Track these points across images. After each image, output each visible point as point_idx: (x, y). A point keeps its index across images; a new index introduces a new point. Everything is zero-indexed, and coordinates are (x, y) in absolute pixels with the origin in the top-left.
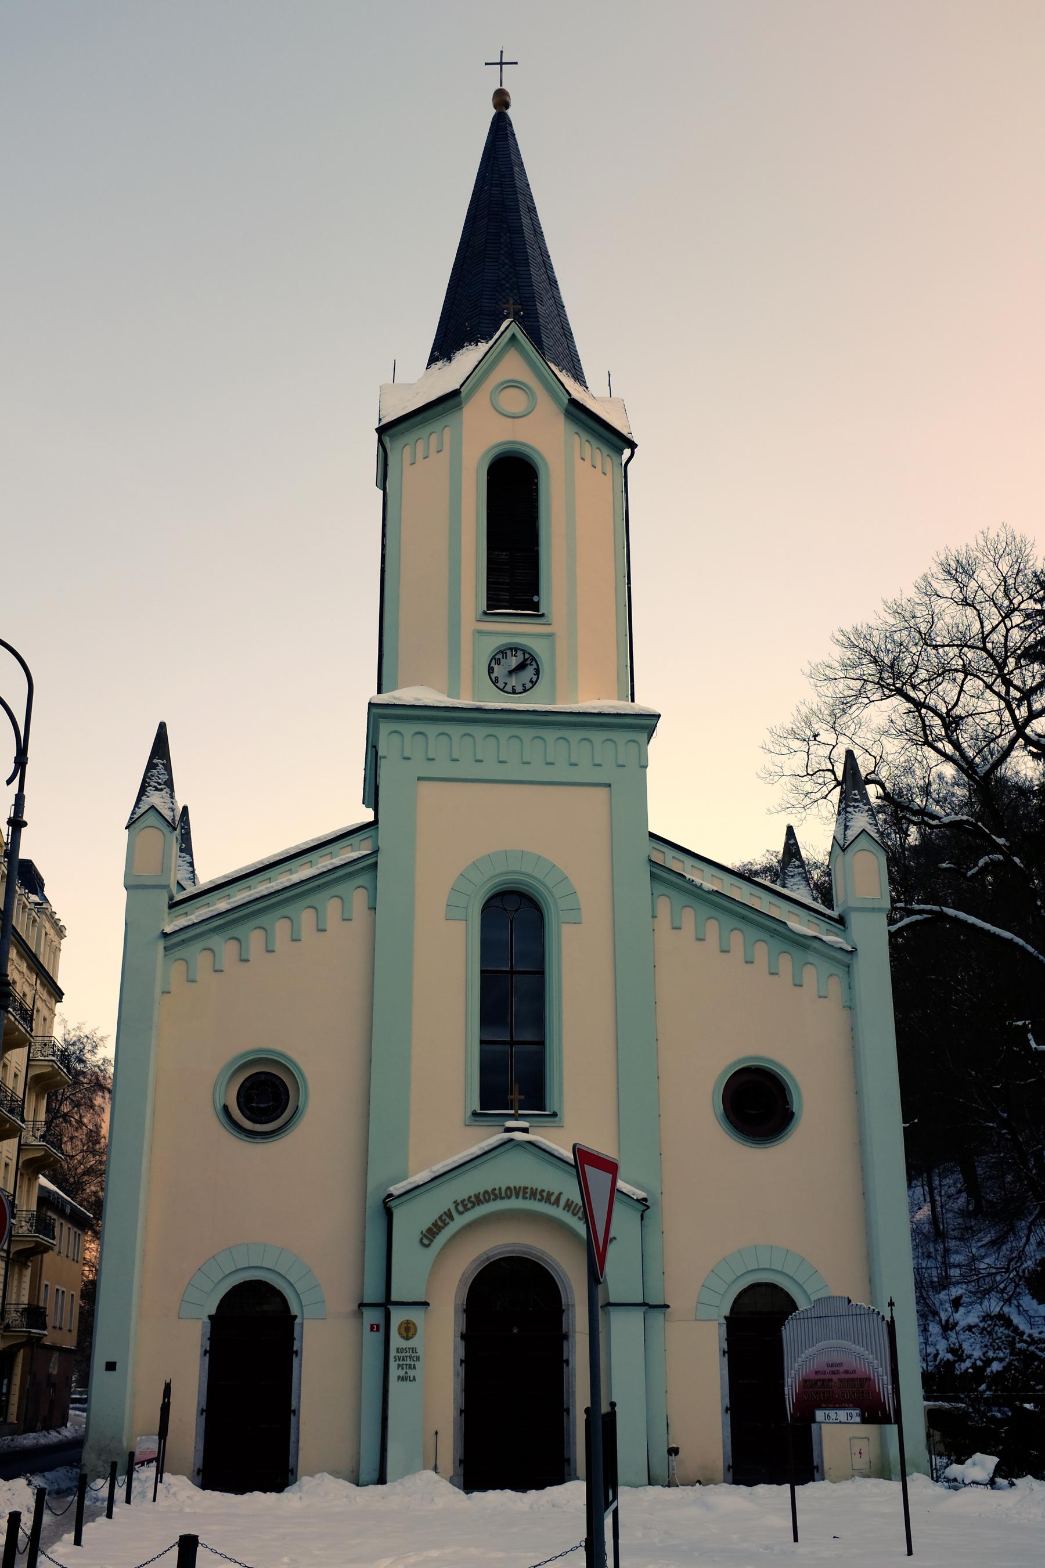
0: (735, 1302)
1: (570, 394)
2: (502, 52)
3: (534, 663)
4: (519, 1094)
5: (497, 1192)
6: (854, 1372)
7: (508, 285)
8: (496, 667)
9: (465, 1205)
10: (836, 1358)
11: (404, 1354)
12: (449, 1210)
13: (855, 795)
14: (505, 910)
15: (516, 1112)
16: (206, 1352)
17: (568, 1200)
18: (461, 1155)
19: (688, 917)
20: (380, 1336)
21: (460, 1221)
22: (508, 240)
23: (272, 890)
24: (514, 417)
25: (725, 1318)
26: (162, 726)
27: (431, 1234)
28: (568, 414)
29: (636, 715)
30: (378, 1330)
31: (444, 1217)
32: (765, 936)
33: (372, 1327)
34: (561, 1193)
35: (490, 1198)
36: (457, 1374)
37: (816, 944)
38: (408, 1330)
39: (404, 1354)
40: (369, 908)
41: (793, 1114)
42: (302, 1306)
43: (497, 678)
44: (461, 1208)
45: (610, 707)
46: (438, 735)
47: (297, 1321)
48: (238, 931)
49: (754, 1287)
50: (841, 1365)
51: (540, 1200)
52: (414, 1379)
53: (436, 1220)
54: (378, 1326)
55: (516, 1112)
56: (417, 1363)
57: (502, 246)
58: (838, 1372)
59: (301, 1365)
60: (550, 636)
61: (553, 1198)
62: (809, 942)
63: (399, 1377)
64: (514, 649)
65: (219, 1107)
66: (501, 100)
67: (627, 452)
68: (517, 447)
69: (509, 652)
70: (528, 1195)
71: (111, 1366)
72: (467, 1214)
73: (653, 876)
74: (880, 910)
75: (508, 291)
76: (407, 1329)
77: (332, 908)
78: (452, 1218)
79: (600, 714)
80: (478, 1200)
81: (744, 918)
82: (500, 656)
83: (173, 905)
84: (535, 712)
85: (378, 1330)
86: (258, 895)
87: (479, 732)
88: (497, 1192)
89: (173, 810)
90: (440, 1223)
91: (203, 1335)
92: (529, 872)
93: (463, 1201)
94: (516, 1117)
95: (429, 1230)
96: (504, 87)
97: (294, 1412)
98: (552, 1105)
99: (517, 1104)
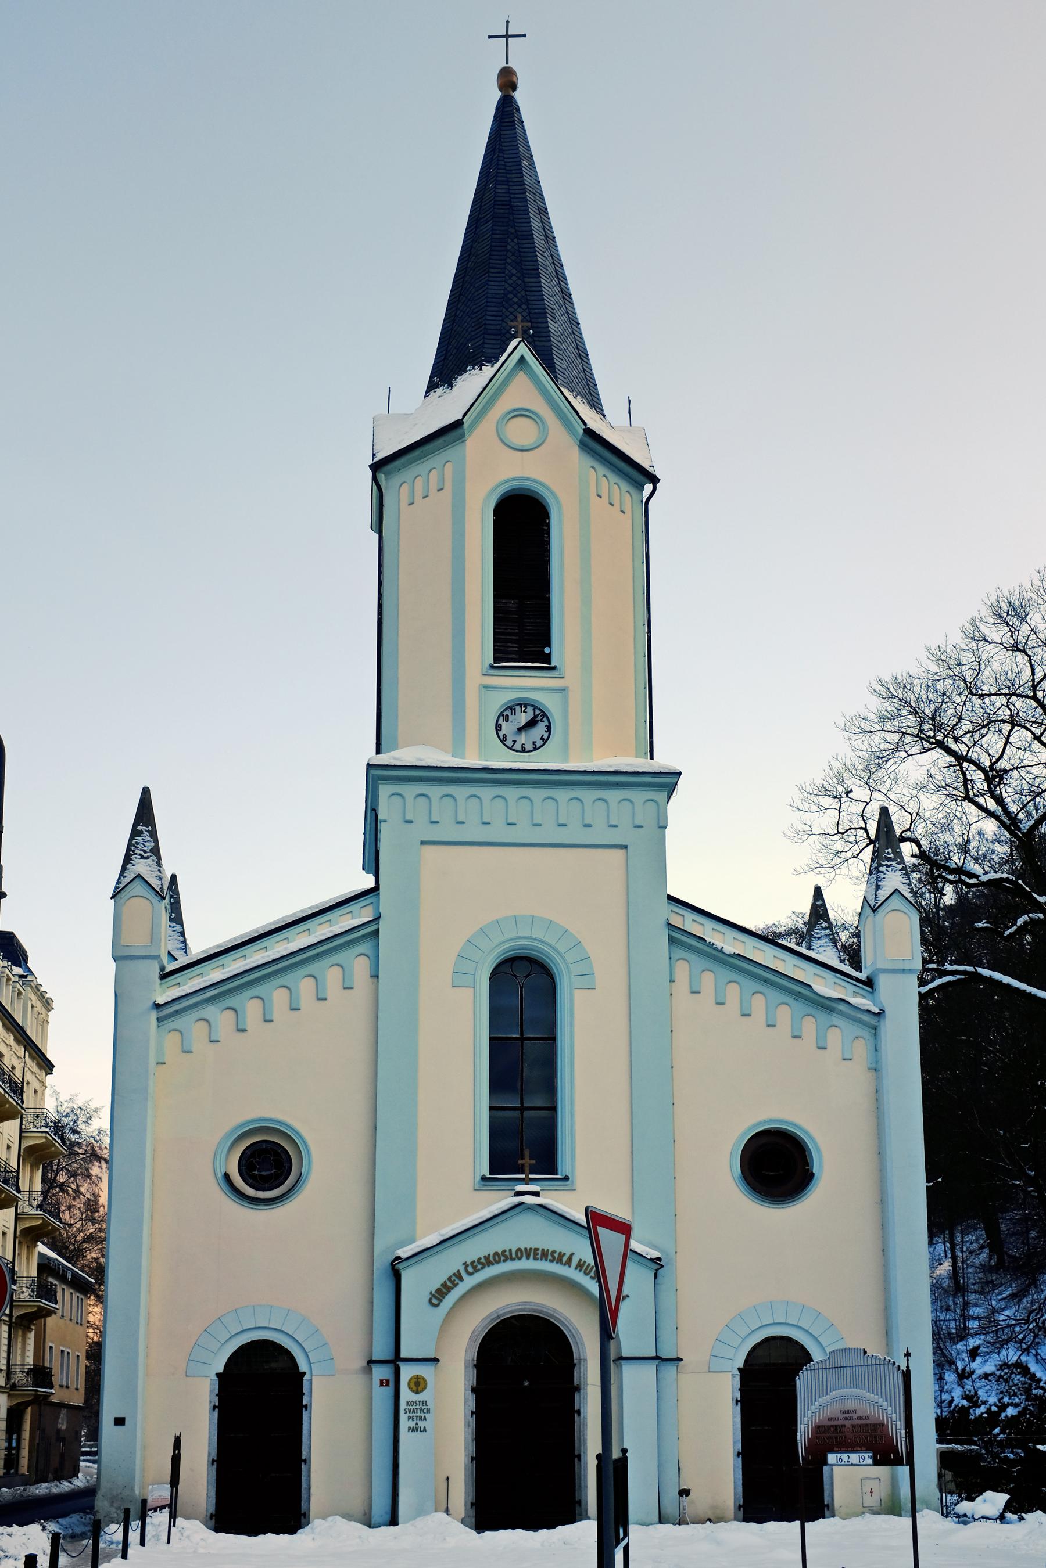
0: (749, 1355)
2: (508, 22)
3: (545, 719)
5: (507, 1253)
6: (868, 1418)
7: (516, 300)
8: (504, 724)
9: (474, 1267)
10: (849, 1405)
11: (414, 1407)
13: (888, 853)
14: (515, 976)
15: (527, 1176)
16: (215, 1407)
17: (580, 1260)
19: (708, 981)
20: (389, 1390)
21: (469, 1282)
22: (516, 247)
24: (522, 451)
25: (739, 1369)
26: (146, 792)
27: (440, 1294)
28: (583, 445)
30: (387, 1385)
31: (453, 1278)
32: (789, 999)
33: (381, 1382)
34: (572, 1254)
35: (500, 1259)
36: (467, 1425)
37: (842, 1007)
38: (418, 1384)
39: (414, 1407)
40: (371, 977)
41: (813, 1175)
42: (310, 1364)
43: (505, 736)
44: (470, 1269)
47: (306, 1378)
48: (233, 1001)
50: (854, 1411)
51: (552, 1261)
53: (445, 1282)
54: (387, 1381)
55: (527, 1176)
57: (509, 254)
58: (851, 1419)
60: (563, 690)
62: (834, 1005)
63: (409, 1428)
64: (524, 705)
65: (220, 1175)
66: (507, 80)
67: (648, 488)
69: (518, 709)
70: (539, 1256)
72: (476, 1275)
73: (671, 939)
74: (911, 971)
75: (516, 306)
76: (417, 1384)
77: (332, 976)
78: (461, 1279)
79: (616, 773)
80: (488, 1261)
82: (508, 712)
85: (387, 1385)
88: (507, 1253)
89: (160, 879)
90: (449, 1284)
91: (211, 1391)
93: (472, 1263)
95: (438, 1291)
96: (510, 65)
99: (527, 1169)
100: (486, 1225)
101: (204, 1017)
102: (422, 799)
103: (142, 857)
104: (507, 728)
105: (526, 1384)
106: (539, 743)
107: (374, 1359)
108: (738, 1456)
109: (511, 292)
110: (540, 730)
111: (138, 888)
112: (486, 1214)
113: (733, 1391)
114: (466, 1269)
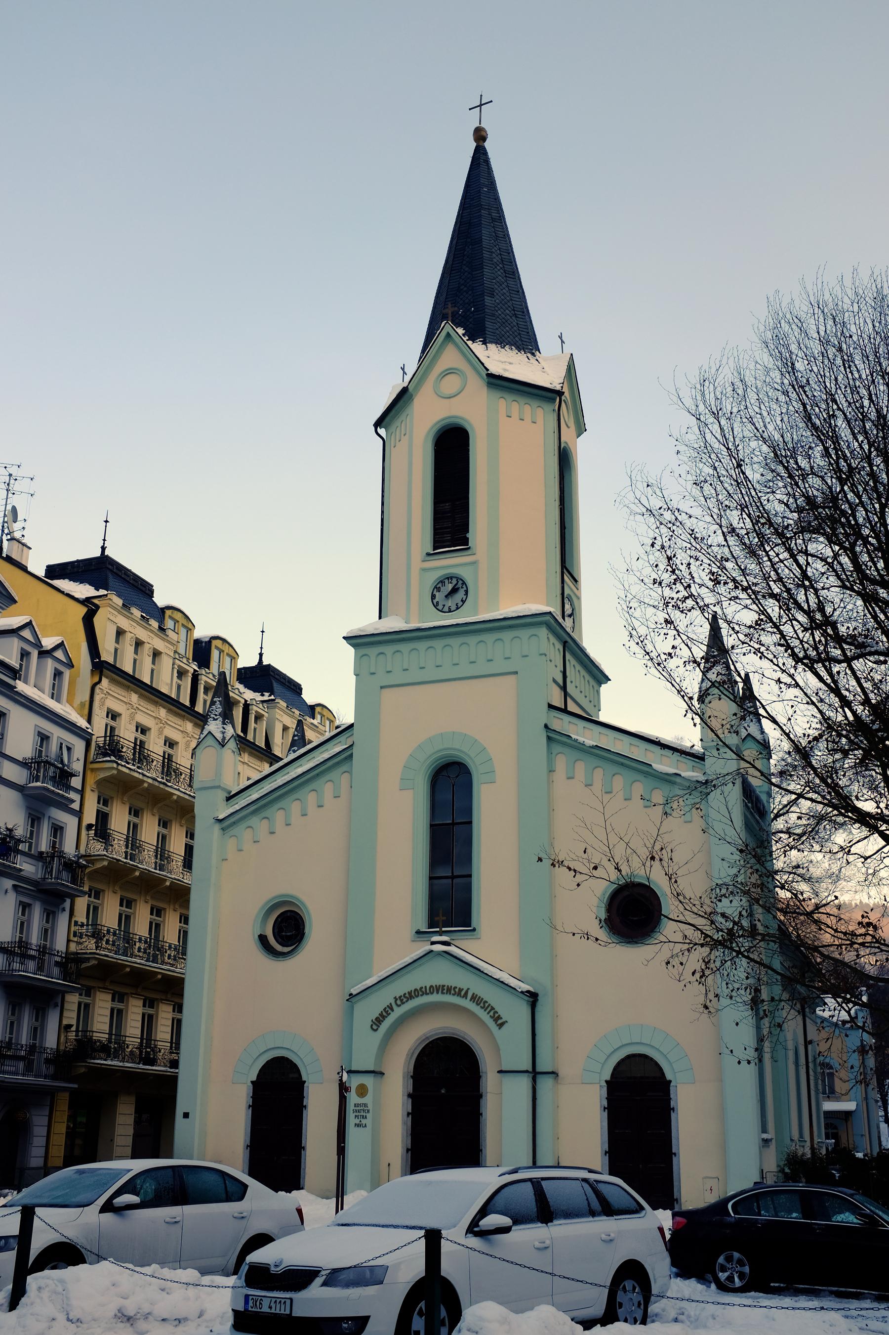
0: (615, 1069)
1: (487, 370)
2: (481, 96)
3: (464, 586)
4: (443, 916)
5: (424, 990)
9: (401, 1000)
11: (359, 1108)
12: (391, 1004)
13: (713, 652)
14: (449, 777)
15: (441, 929)
16: (250, 1106)
17: (474, 994)
18: (397, 964)
19: (581, 768)
21: (398, 1012)
23: (285, 781)
24: (450, 398)
25: (606, 1081)
27: (378, 1021)
28: (490, 385)
29: (532, 615)
31: (387, 1009)
32: (640, 777)
34: (468, 989)
36: (404, 1123)
37: (678, 780)
39: (359, 1108)
43: (438, 603)
44: (399, 1002)
45: (513, 612)
46: (512, 640)
48: (267, 813)
49: (630, 1057)
51: (454, 995)
52: (366, 1126)
55: (441, 929)
56: (368, 1115)
59: (677, 1120)
60: (474, 563)
61: (463, 993)
62: (673, 779)
63: (356, 1124)
64: (450, 578)
66: (480, 135)
68: (444, 422)
69: (446, 581)
70: (445, 991)
71: (186, 1115)
72: (403, 1006)
77: (328, 789)
78: (392, 1010)
79: (505, 619)
81: (622, 764)
83: (228, 799)
84: (457, 625)
86: (276, 786)
87: (422, 645)
89: (223, 733)
90: (384, 1014)
91: (248, 1094)
92: (457, 747)
93: (400, 997)
94: (441, 933)
95: (377, 1019)
96: (482, 125)
97: (675, 1154)
98: (474, 923)
99: (441, 925)
100: (409, 968)
101: (249, 825)
102: (398, 654)
103: (215, 719)
104: (439, 596)
105: (443, 1092)
106: (460, 604)
107: (353, 1069)
108: (606, 1155)
109: (463, 285)
110: (461, 594)
111: (210, 741)
112: (408, 960)
113: (601, 1100)
114: (396, 1001)
